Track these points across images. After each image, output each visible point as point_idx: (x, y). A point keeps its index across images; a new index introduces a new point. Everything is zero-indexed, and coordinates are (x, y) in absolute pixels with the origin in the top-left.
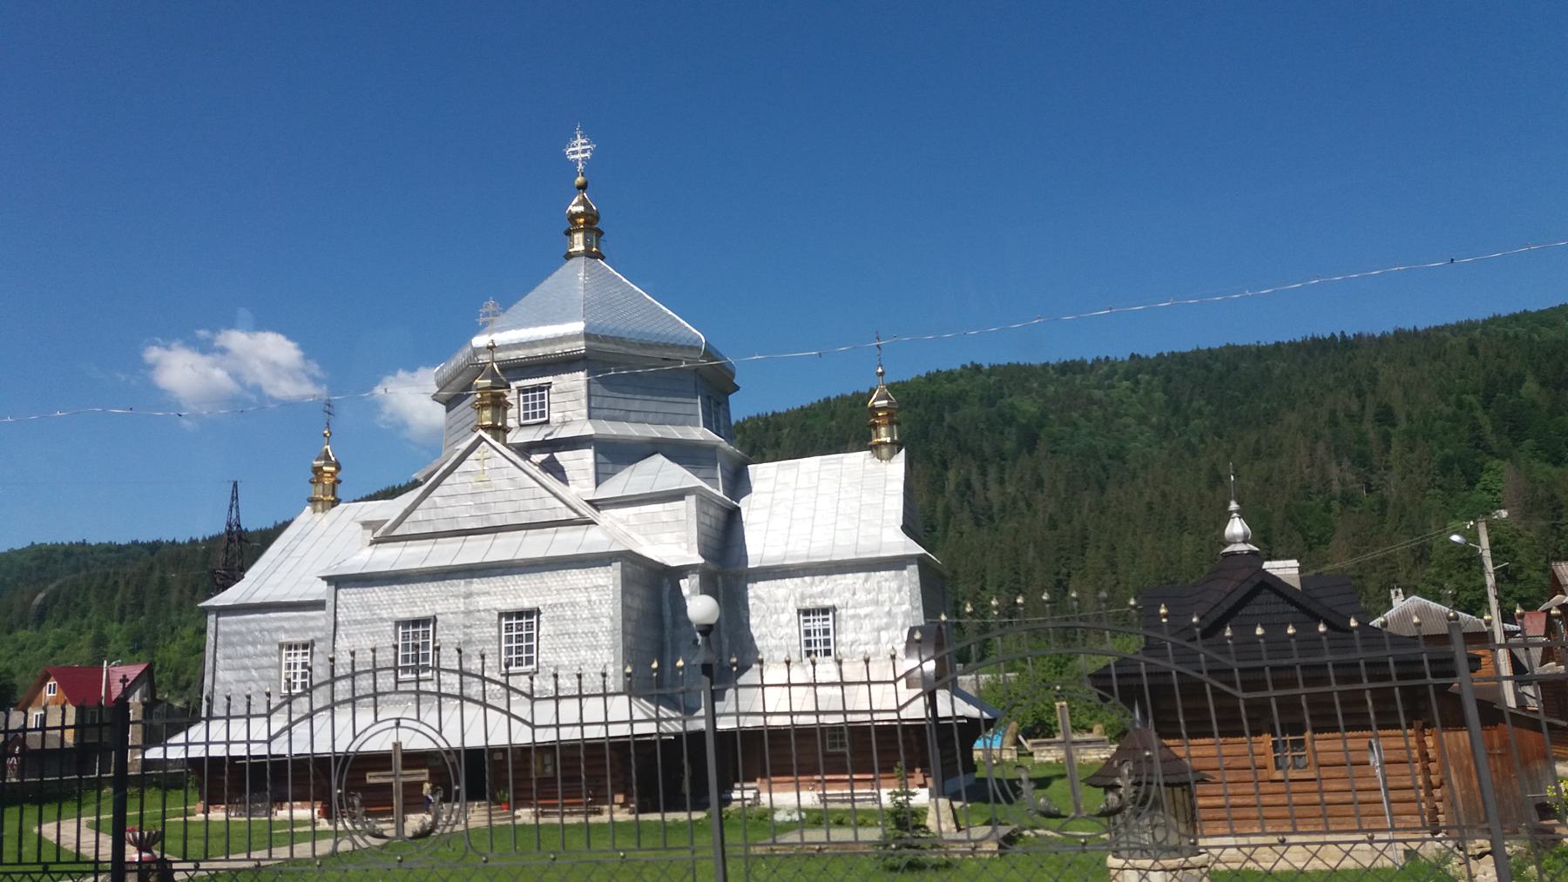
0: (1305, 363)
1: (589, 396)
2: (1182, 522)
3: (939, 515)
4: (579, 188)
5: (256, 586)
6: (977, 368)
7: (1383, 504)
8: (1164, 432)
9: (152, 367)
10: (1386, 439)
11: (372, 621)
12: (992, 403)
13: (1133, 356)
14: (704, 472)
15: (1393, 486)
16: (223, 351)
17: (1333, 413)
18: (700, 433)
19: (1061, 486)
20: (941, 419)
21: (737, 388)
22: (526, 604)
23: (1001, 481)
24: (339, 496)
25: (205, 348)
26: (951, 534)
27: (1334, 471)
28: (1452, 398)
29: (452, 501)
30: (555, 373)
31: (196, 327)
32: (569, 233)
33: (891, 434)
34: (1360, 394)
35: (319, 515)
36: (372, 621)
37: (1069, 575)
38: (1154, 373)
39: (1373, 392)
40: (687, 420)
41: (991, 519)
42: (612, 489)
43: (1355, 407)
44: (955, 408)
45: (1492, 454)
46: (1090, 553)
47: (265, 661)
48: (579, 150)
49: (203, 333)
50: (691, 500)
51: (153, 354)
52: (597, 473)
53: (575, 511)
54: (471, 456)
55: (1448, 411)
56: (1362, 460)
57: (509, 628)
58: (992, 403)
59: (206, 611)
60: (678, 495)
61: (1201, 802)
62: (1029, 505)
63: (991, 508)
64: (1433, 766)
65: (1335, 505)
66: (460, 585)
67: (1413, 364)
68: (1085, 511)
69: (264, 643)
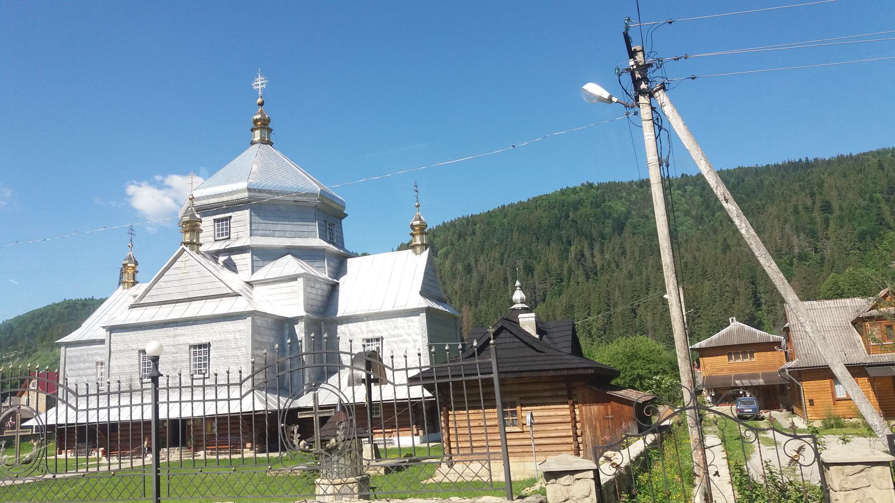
0: (783, 177)
1: (251, 223)
2: (704, 273)
3: (565, 273)
4: (259, 105)
6: (591, 186)
7: (823, 259)
8: (700, 219)
9: (131, 197)
10: (827, 221)
11: (128, 350)
12: (598, 206)
13: (683, 175)
14: (317, 264)
15: (829, 249)
16: (169, 187)
17: (796, 207)
18: (317, 242)
19: (637, 254)
20: (567, 216)
22: (204, 341)
23: (602, 252)
24: (137, 280)
25: (160, 186)
26: (572, 283)
27: (795, 241)
28: (867, 196)
29: (169, 284)
31: (153, 172)
32: (252, 130)
33: (422, 239)
34: (812, 195)
35: (126, 290)
36: (128, 350)
37: (639, 306)
38: (695, 185)
39: (820, 193)
40: (309, 235)
41: (596, 274)
42: (260, 275)
43: (809, 203)
44: (576, 209)
45: (890, 228)
46: (651, 292)
47: (89, 372)
48: (259, 83)
49: (159, 178)
51: (132, 189)
52: (253, 266)
55: (864, 203)
56: (813, 234)
58: (598, 206)
59: (60, 345)
60: (293, 278)
61: (499, 443)
62: (617, 266)
63: (595, 268)
64: (578, 425)
65: (795, 260)
66: (171, 331)
67: (845, 176)
68: (650, 268)
69: (90, 362)
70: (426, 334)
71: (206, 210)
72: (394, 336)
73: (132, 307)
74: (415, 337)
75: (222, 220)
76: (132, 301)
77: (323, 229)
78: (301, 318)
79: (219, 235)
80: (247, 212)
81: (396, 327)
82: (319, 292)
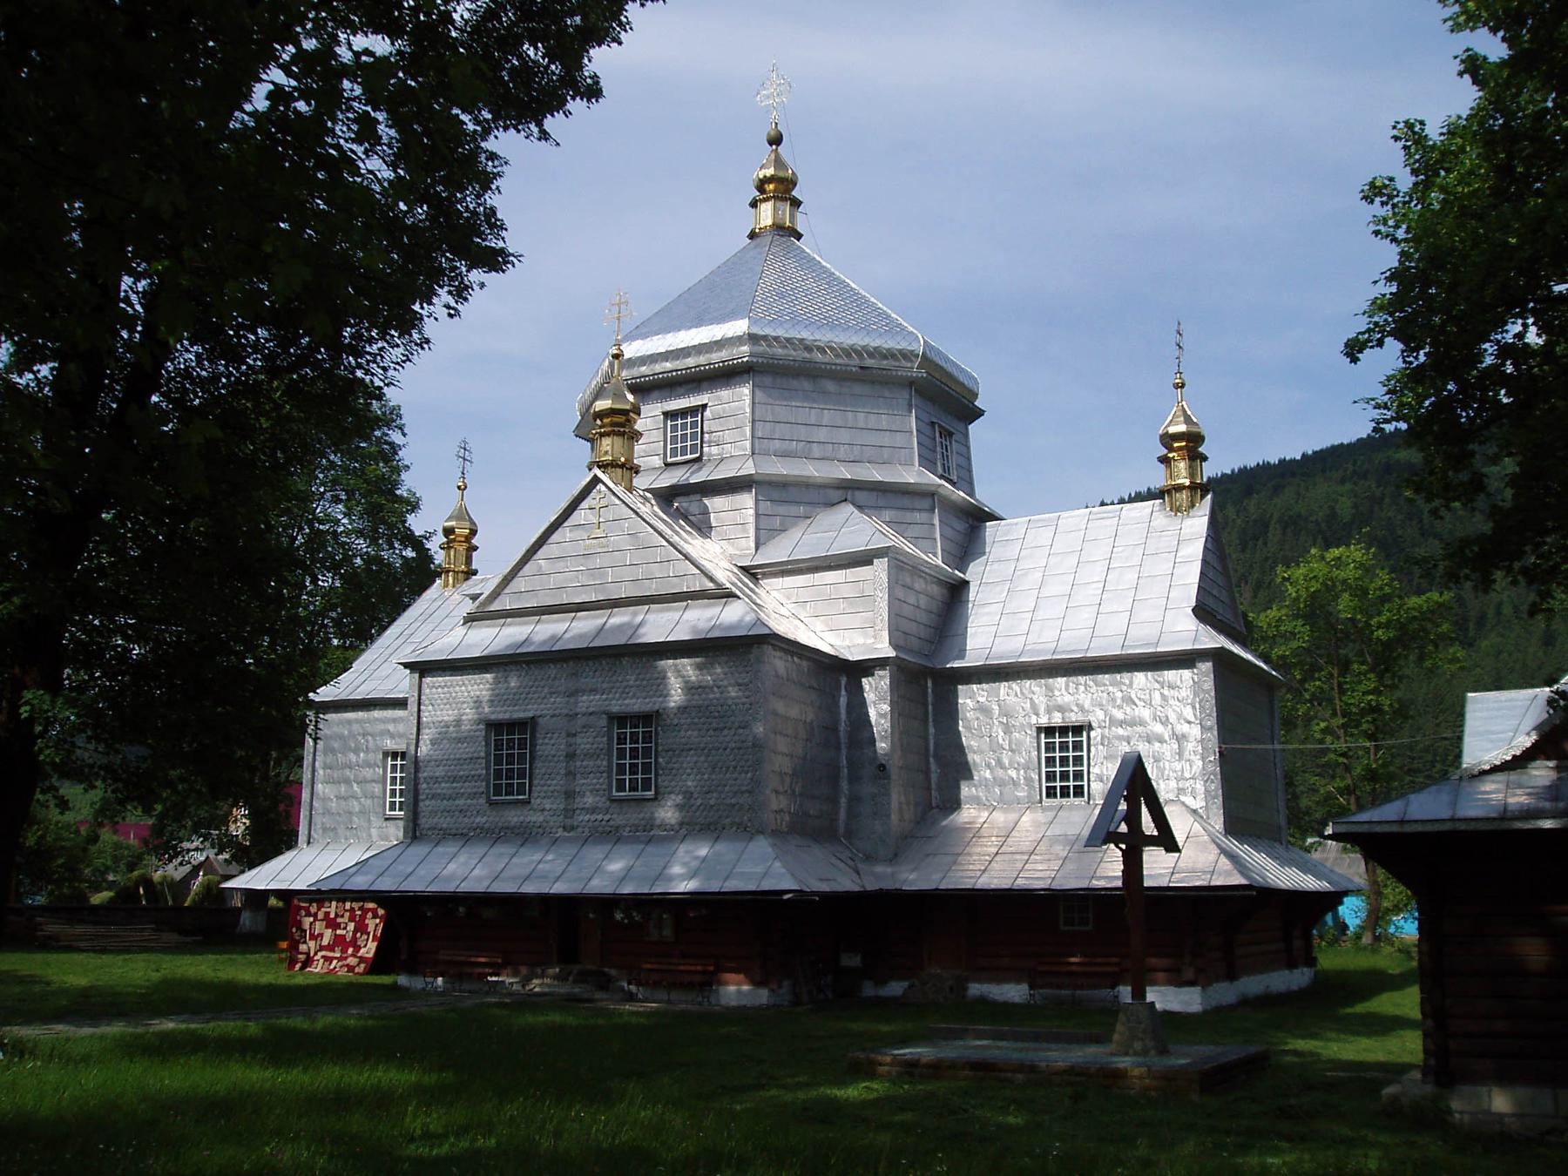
5: (362, 679)
18: (914, 474)
21: (979, 413)
29: (560, 565)
30: (711, 389)
32: (754, 204)
47: (368, 773)
50: (879, 571)
53: (711, 579)
54: (585, 504)
57: (1050, 747)
59: (311, 704)
60: (863, 559)
70: (1211, 722)
71: (645, 389)
72: (1121, 723)
73: (470, 619)
74: (1183, 728)
75: (683, 413)
76: (469, 607)
77: (927, 442)
78: (881, 663)
79: (674, 452)
80: (746, 391)
81: (1129, 701)
82: (923, 601)
